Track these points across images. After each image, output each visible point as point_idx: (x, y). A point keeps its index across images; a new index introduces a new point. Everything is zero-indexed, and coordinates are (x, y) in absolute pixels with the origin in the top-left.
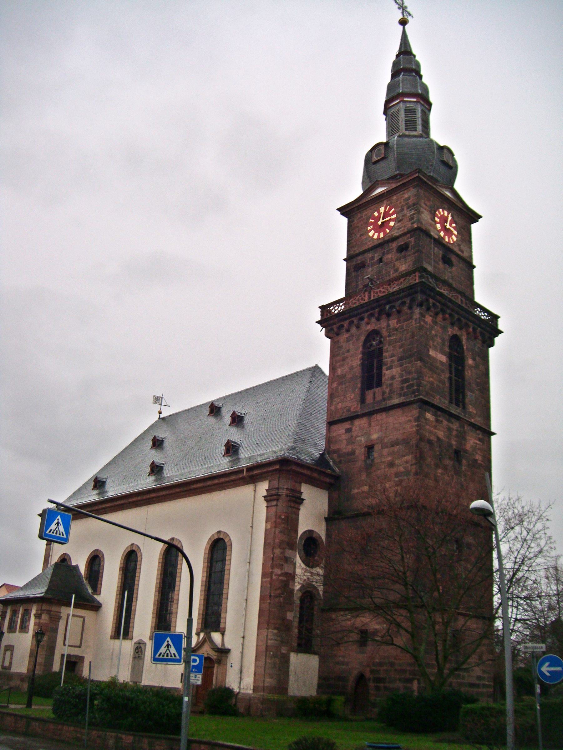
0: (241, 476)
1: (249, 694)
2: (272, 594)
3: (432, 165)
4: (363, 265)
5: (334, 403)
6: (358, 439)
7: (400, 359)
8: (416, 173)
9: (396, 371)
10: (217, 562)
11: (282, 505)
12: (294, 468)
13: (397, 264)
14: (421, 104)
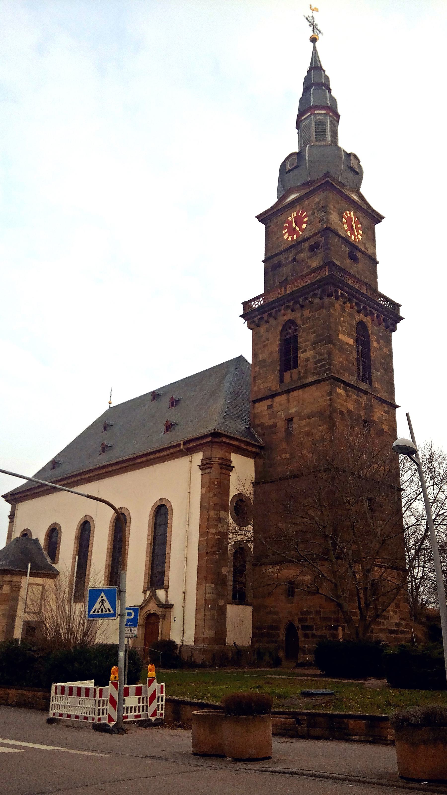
0: (178, 449)
1: (190, 646)
2: (209, 552)
3: (340, 171)
4: (278, 266)
5: (257, 384)
6: (279, 413)
7: (313, 343)
8: (326, 178)
9: (309, 354)
10: (160, 525)
11: (215, 471)
12: (224, 439)
13: (309, 262)
14: (330, 116)
